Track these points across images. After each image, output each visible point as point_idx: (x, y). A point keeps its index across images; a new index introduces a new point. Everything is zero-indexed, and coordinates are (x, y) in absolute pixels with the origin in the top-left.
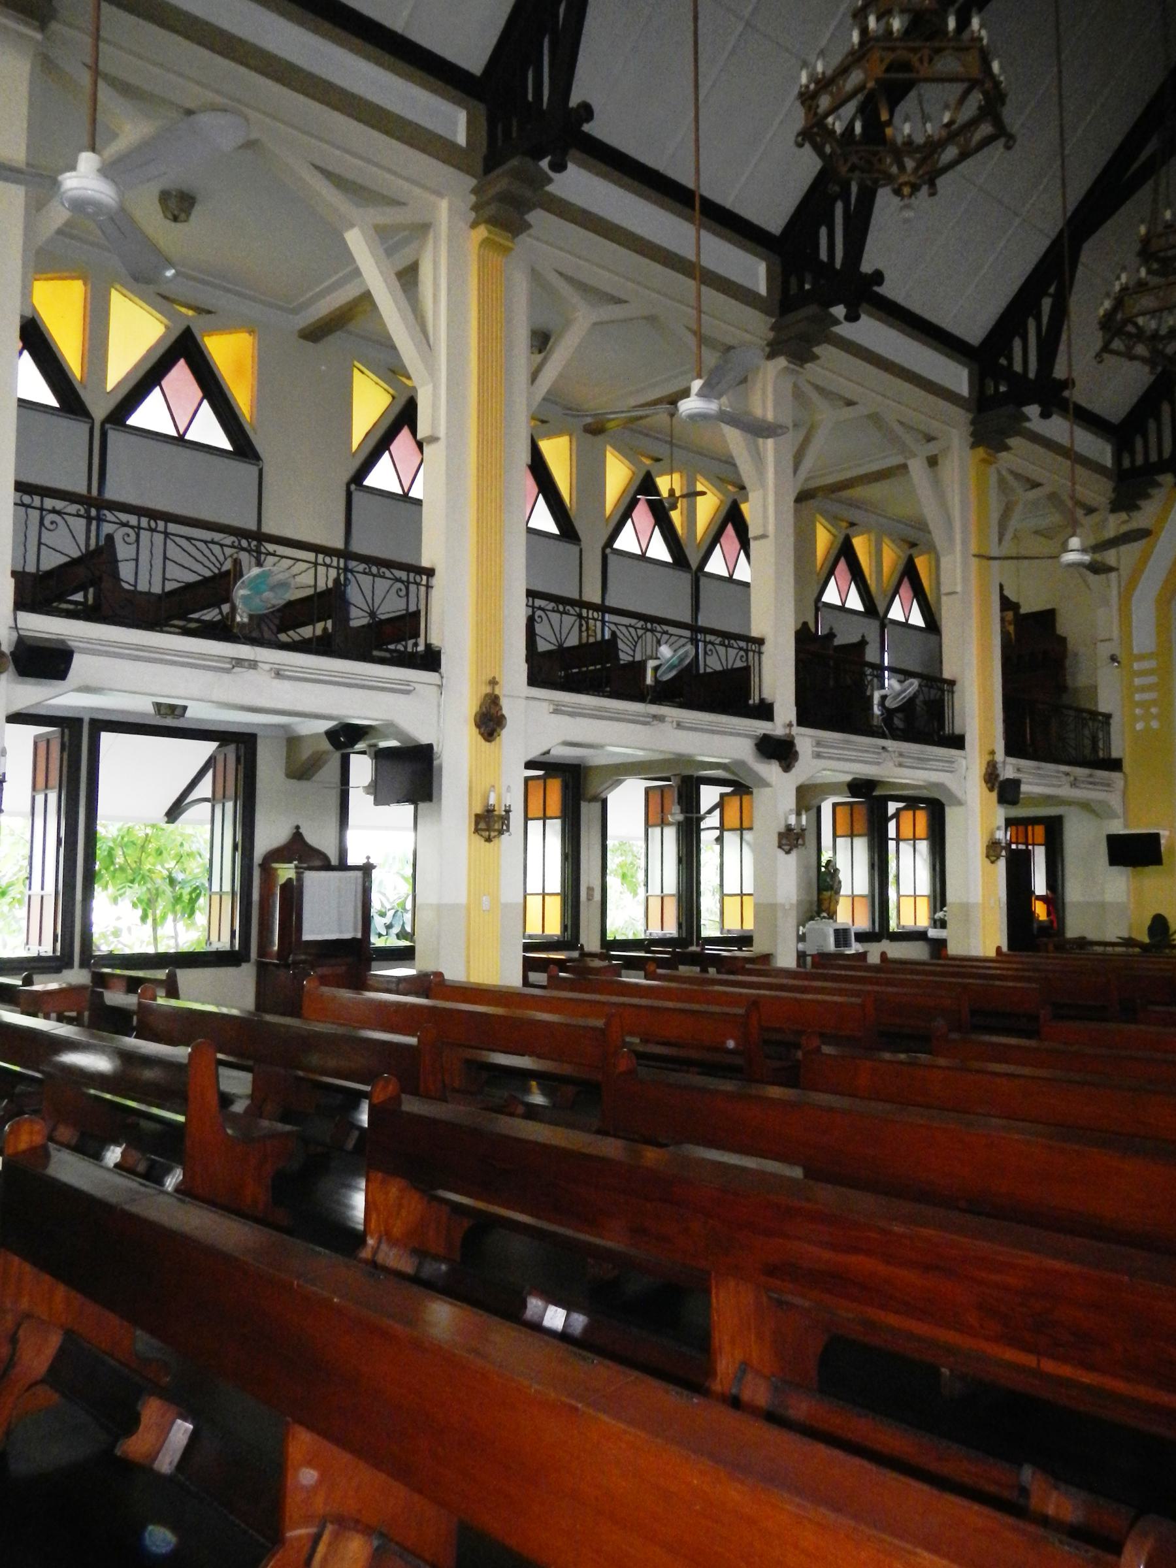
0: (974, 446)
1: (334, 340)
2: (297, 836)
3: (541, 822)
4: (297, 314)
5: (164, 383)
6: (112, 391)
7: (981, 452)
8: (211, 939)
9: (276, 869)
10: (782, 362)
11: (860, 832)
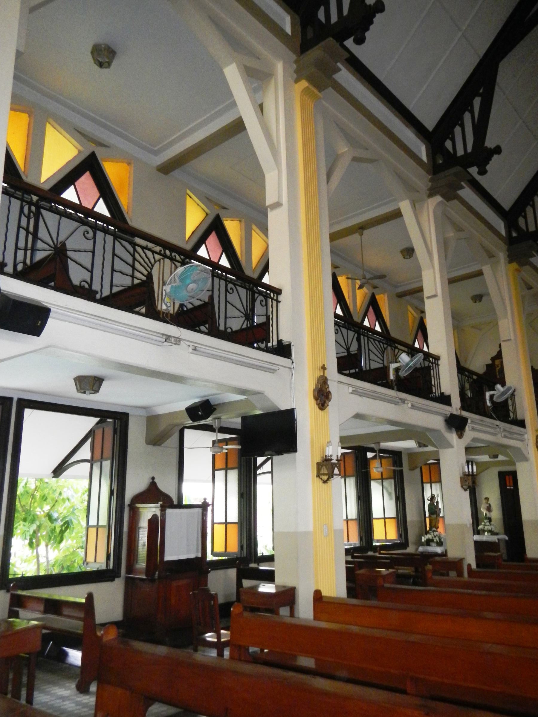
0: (510, 262)
1: (176, 173)
2: (153, 484)
4: (156, 155)
5: (77, 183)
6: (43, 183)
7: (515, 265)
8: (88, 560)
9: (138, 508)
10: (438, 199)
11: (221, 467)
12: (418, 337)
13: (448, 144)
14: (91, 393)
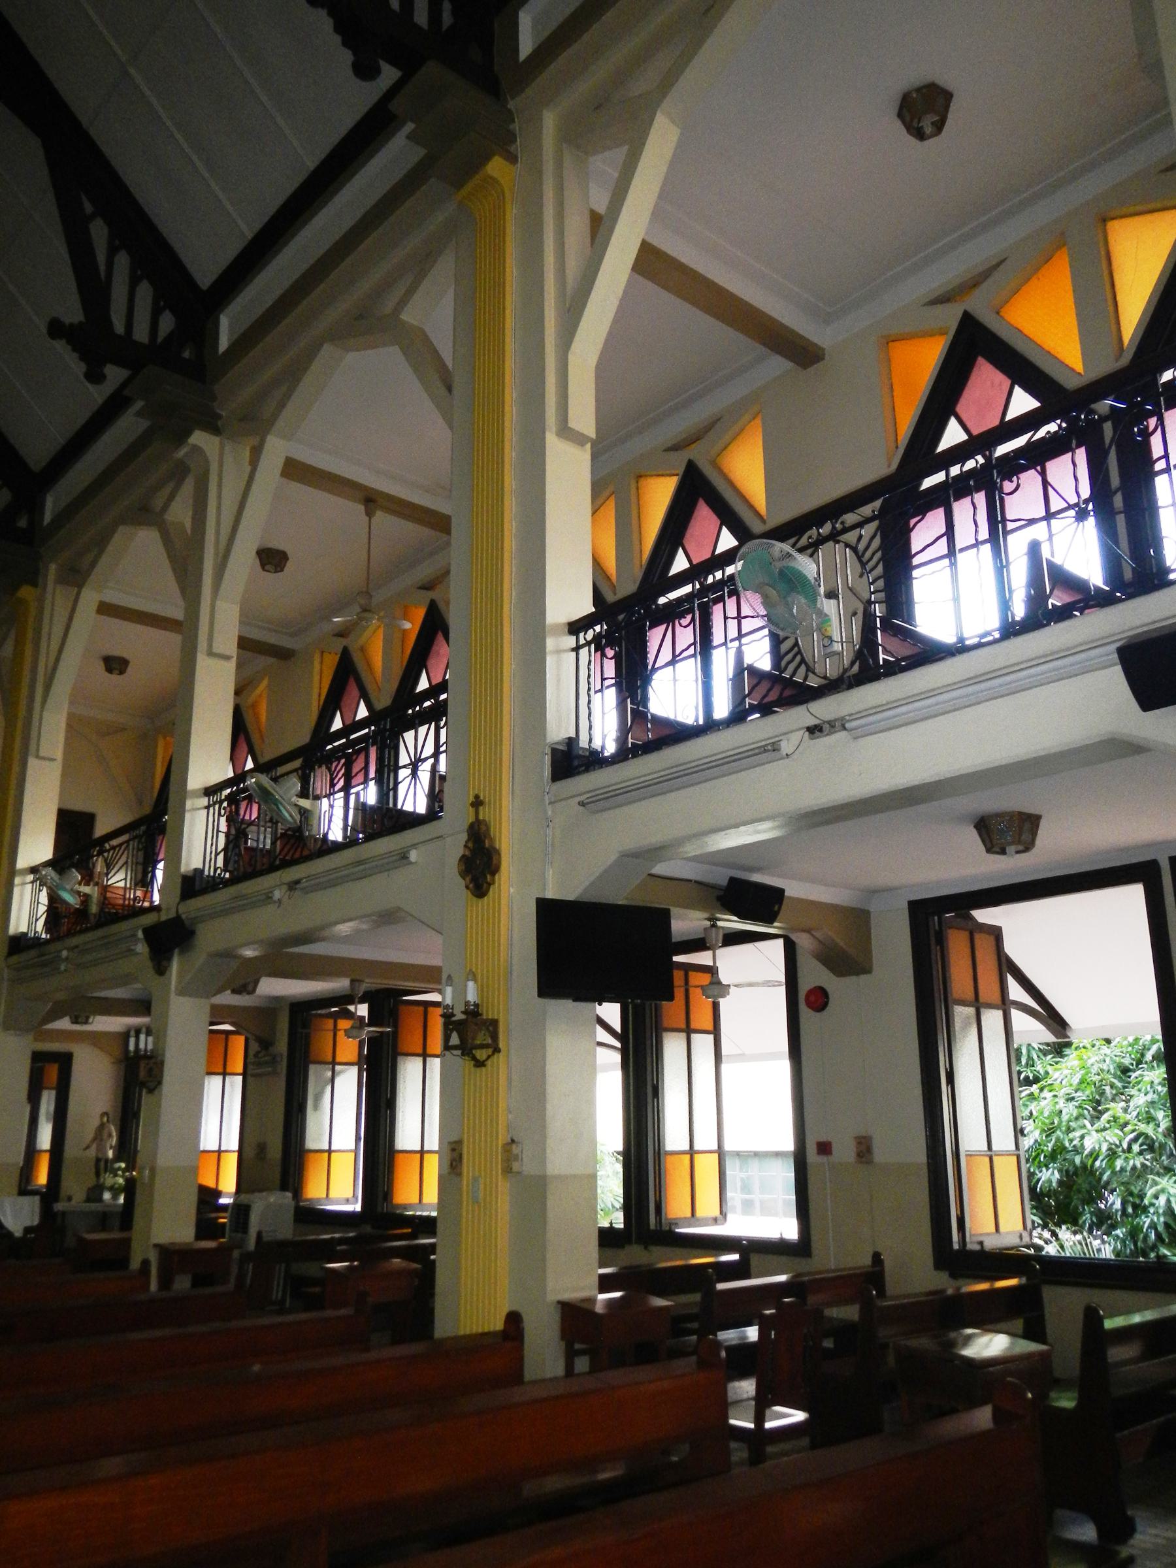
5: (959, 409)
14: (1017, 852)
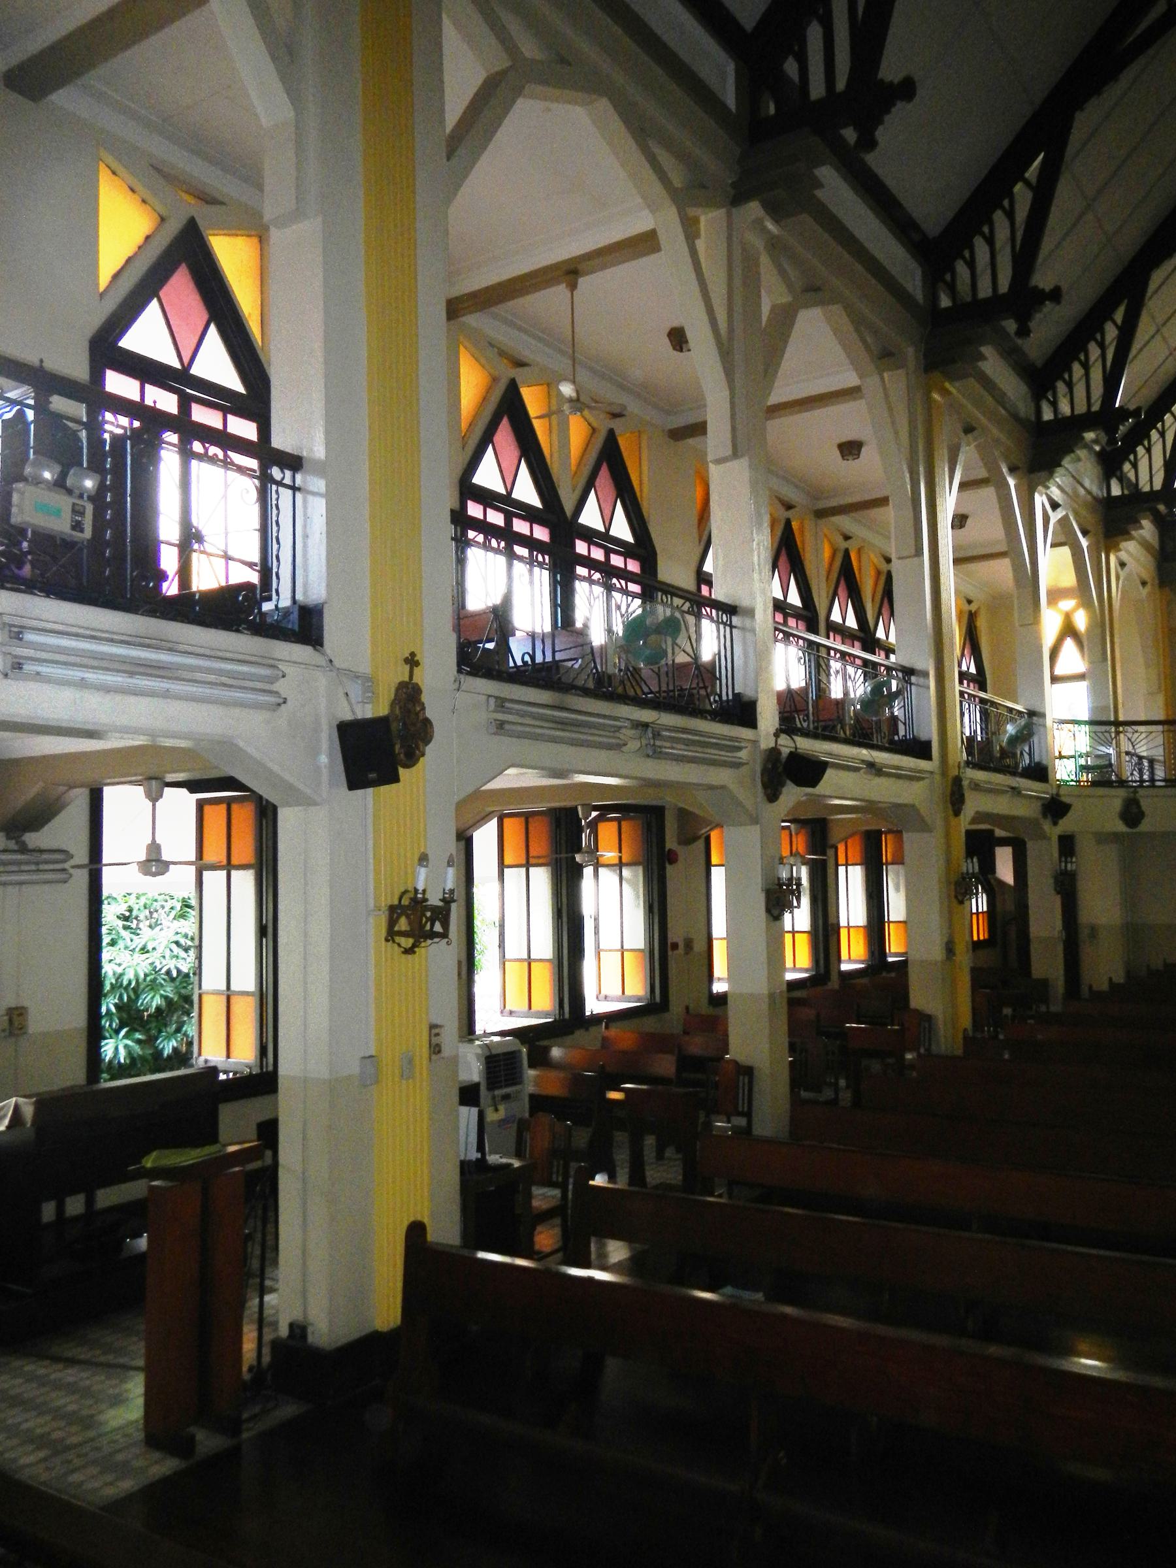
3: (523, 870)
11: (244, 862)
12: (597, 484)
13: (791, 67)
